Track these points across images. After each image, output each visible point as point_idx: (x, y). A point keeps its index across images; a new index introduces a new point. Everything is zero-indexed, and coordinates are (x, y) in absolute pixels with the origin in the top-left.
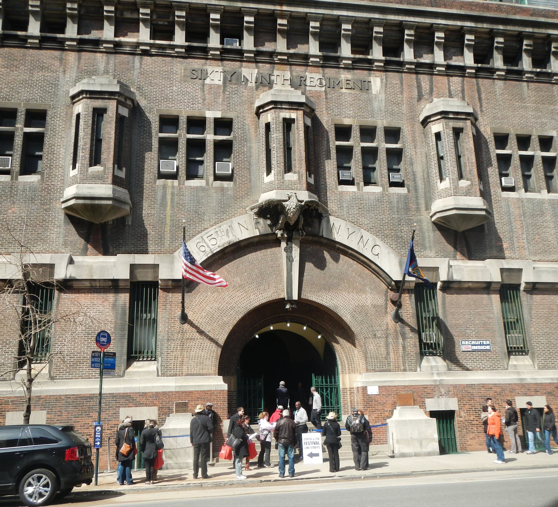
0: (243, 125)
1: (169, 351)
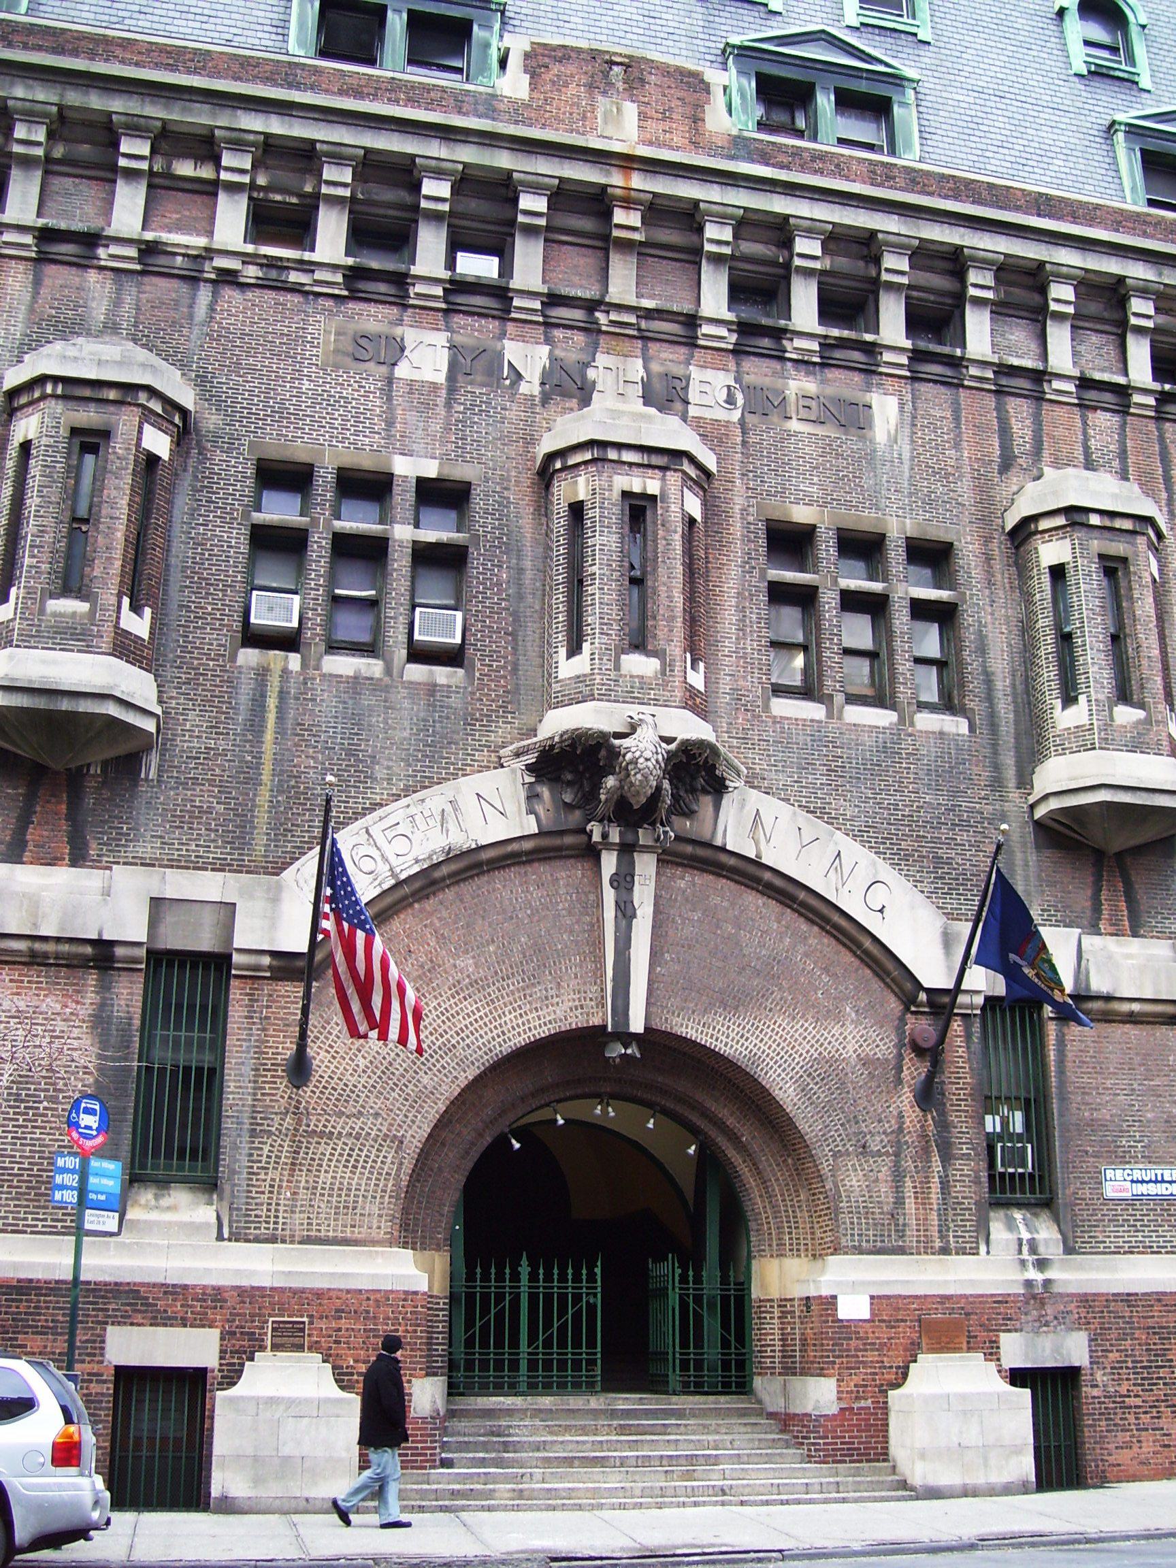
0: (500, 504)
1: (255, 1165)
